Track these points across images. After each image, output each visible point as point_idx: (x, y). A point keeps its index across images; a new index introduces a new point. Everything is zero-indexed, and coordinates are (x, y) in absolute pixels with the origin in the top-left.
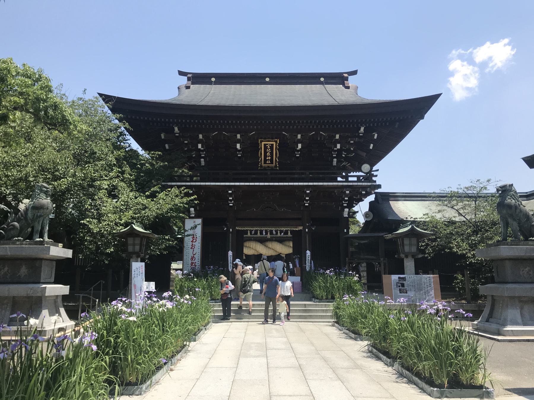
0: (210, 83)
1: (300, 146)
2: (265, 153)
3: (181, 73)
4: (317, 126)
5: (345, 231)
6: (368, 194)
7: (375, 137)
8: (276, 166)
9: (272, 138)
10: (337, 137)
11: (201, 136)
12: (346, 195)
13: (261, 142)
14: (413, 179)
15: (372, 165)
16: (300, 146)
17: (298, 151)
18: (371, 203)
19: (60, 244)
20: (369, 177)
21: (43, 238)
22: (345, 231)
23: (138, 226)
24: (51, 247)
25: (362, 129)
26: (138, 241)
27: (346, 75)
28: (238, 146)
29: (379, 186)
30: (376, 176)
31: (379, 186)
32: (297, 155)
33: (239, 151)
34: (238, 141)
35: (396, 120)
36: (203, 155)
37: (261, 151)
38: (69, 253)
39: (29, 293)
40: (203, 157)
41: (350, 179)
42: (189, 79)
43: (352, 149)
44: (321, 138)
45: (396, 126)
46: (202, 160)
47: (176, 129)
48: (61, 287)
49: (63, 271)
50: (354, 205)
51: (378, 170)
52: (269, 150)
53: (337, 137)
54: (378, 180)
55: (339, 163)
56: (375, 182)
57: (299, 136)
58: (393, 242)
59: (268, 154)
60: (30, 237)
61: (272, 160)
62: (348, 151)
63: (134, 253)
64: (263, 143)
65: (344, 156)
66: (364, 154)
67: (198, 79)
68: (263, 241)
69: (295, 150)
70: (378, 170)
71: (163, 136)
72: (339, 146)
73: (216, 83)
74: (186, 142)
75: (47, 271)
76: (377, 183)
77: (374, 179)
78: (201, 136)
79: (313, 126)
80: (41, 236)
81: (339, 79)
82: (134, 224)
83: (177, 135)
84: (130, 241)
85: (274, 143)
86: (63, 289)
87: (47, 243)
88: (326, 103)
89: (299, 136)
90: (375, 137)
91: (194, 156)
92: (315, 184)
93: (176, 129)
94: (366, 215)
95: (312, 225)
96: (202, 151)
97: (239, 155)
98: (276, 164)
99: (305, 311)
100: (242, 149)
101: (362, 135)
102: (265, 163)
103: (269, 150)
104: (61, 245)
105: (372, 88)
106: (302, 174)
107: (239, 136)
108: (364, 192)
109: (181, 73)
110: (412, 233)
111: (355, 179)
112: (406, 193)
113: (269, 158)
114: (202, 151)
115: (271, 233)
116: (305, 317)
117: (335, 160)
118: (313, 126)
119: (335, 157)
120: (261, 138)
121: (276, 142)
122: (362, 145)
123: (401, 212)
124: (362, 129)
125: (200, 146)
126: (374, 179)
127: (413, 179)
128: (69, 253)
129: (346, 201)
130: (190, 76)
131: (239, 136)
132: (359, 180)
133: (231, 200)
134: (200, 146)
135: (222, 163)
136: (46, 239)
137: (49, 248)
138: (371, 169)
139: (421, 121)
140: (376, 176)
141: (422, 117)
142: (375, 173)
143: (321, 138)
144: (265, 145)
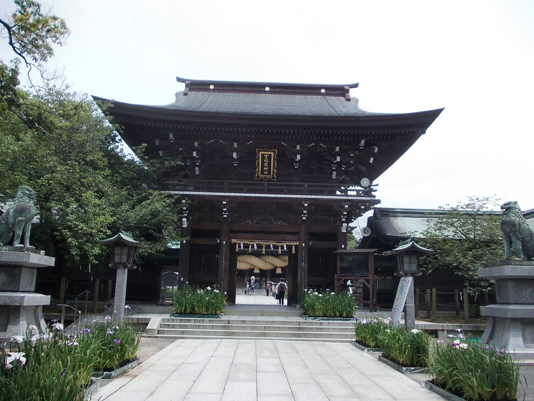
0: (209, 90)
1: (299, 157)
2: (263, 163)
3: (179, 80)
4: (317, 137)
5: (343, 246)
6: (367, 209)
7: (376, 151)
8: (273, 177)
9: (270, 149)
10: (337, 149)
11: (196, 144)
12: (345, 210)
14: (410, 188)
15: (372, 179)
16: (299, 157)
17: (297, 162)
18: (369, 219)
19: (42, 251)
20: (368, 191)
21: (236, 244)
22: (343, 246)
23: (127, 235)
24: (31, 253)
25: (363, 142)
26: (125, 251)
27: (347, 88)
28: (235, 155)
29: (379, 202)
30: (376, 191)
31: (379, 202)
32: (296, 167)
33: (236, 160)
34: (235, 150)
35: (398, 133)
37: (259, 162)
38: (51, 261)
39: (6, 302)
40: (197, 166)
41: (350, 193)
42: (187, 86)
43: (352, 162)
45: (397, 140)
46: (197, 168)
47: (171, 136)
48: (42, 297)
49: (45, 281)
50: (353, 220)
51: (377, 185)
52: (266, 161)
53: (337, 149)
54: (378, 195)
55: (339, 177)
56: (374, 196)
57: (298, 147)
58: (393, 258)
60: (10, 243)
61: (269, 171)
62: (348, 164)
63: (120, 263)
65: (343, 169)
66: (364, 168)
67: (195, 86)
68: (258, 254)
69: (293, 161)
70: (377, 185)
71: (157, 143)
72: (338, 159)
73: (214, 90)
74: (181, 149)
75: (28, 280)
77: (373, 193)
78: (196, 144)
79: (313, 137)
80: (22, 242)
81: (341, 91)
82: (122, 233)
84: (117, 250)
85: (272, 153)
86: (45, 299)
87: (28, 250)
88: (326, 114)
89: (298, 147)
90: (376, 151)
91: (188, 164)
92: (313, 197)
93: (171, 136)
94: (364, 230)
95: (309, 240)
96: (198, 159)
97: (235, 165)
98: (273, 175)
99: (299, 329)
100: (239, 158)
101: (362, 148)
102: (262, 173)
103: (266, 161)
104: (43, 252)
105: (374, 100)
106: (301, 186)
107: (235, 145)
108: (363, 207)
109: (179, 80)
110: (413, 251)
111: (354, 193)
113: (267, 168)
114: (198, 159)
115: (268, 247)
116: (299, 335)
117: (335, 173)
118: (313, 137)
119: (334, 170)
121: (274, 152)
122: (362, 159)
123: (399, 228)
124: (363, 142)
125: (195, 154)
126: (373, 193)
127: (410, 188)
128: (51, 261)
129: (345, 215)
130: (188, 82)
131: (235, 145)
132: (358, 195)
133: (225, 212)
134: (195, 154)
135: (217, 171)
136: (28, 245)
137: (29, 255)
138: (371, 183)
139: (423, 135)
140: (376, 191)
141: (424, 132)
142: (374, 188)
144: (263, 155)
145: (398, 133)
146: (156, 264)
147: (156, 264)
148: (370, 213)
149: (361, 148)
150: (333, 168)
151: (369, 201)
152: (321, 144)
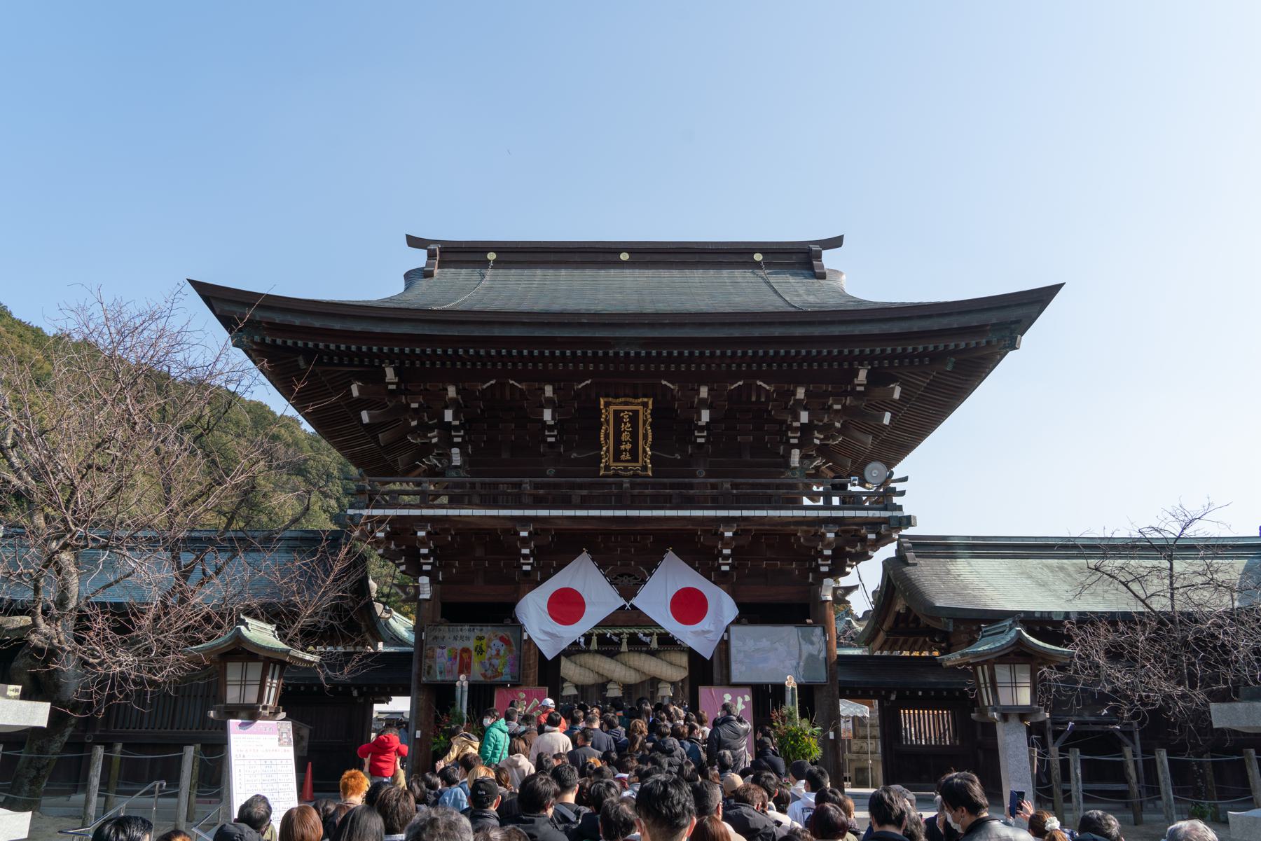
2: (618, 433)
7: (897, 395)
10: (801, 393)
13: (607, 405)
14: (988, 485)
25: (862, 375)
28: (547, 415)
35: (949, 350)
36: (459, 440)
44: (758, 396)
51: (905, 479)
56: (900, 508)
57: (704, 392)
59: (625, 436)
64: (612, 408)
76: (906, 512)
81: (802, 258)
83: (394, 387)
85: (640, 408)
89: (704, 392)
92: (746, 513)
96: (457, 428)
101: (862, 389)
102: (617, 458)
112: (974, 538)
113: (629, 446)
114: (457, 428)
119: (794, 446)
120: (607, 396)
121: (645, 405)
124: (862, 375)
131: (549, 391)
134: (448, 415)
143: (758, 396)
144: (616, 413)
145: (949, 350)
146: (355, 693)
147: (355, 693)
148: (889, 551)
149: (391, 387)
150: (792, 441)
151: (886, 521)
152: (664, 382)
